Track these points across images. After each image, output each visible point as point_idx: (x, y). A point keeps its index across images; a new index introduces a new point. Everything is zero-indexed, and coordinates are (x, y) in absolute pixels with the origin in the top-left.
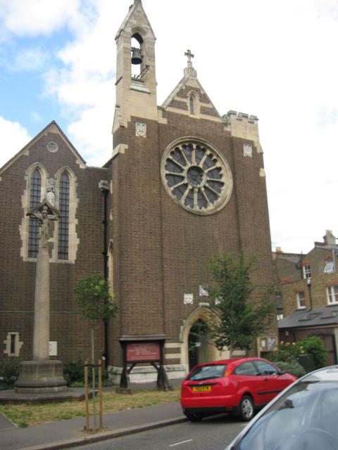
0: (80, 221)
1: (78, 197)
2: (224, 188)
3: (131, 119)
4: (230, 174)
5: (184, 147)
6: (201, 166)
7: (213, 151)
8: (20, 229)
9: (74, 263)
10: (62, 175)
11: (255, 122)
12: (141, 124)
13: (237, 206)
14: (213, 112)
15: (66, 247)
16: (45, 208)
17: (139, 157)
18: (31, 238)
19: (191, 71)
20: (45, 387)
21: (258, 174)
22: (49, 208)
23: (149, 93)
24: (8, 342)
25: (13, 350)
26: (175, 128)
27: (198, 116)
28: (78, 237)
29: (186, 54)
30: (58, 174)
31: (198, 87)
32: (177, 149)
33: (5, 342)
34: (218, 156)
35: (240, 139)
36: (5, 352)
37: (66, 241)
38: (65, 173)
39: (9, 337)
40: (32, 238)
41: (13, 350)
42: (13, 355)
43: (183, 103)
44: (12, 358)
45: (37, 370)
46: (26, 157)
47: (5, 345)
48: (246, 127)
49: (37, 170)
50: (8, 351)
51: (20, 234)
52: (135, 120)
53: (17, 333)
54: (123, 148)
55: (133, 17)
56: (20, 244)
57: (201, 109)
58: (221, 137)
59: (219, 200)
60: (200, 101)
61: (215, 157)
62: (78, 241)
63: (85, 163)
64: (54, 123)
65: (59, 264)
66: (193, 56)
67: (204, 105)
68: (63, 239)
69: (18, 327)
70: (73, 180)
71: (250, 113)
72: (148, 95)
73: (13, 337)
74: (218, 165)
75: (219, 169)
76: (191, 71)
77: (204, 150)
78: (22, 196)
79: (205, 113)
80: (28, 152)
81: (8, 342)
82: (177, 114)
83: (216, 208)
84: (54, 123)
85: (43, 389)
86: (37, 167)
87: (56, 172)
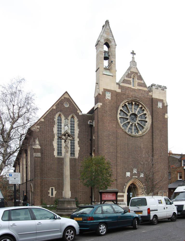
0: (80, 139)
1: (79, 128)
4: (150, 117)
6: (136, 113)
9: (77, 158)
10: (71, 118)
11: (165, 89)
13: (153, 132)
15: (74, 151)
16: (67, 134)
18: (58, 147)
20: (69, 209)
23: (112, 76)
25: (52, 194)
26: (124, 94)
27: (137, 87)
28: (79, 147)
30: (70, 118)
34: (145, 108)
36: (49, 195)
37: (74, 148)
38: (73, 117)
39: (50, 189)
40: (58, 131)
41: (52, 194)
42: (52, 196)
45: (66, 203)
46: (54, 109)
47: (49, 192)
48: (160, 93)
50: (50, 195)
51: (54, 145)
53: (54, 188)
61: (143, 108)
62: (79, 148)
64: (66, 92)
65: (59, 158)
67: (139, 81)
72: (112, 77)
73: (52, 189)
74: (145, 112)
75: (145, 114)
76: (133, 63)
77: (138, 105)
80: (55, 107)
82: (125, 87)
84: (66, 92)
85: (68, 210)
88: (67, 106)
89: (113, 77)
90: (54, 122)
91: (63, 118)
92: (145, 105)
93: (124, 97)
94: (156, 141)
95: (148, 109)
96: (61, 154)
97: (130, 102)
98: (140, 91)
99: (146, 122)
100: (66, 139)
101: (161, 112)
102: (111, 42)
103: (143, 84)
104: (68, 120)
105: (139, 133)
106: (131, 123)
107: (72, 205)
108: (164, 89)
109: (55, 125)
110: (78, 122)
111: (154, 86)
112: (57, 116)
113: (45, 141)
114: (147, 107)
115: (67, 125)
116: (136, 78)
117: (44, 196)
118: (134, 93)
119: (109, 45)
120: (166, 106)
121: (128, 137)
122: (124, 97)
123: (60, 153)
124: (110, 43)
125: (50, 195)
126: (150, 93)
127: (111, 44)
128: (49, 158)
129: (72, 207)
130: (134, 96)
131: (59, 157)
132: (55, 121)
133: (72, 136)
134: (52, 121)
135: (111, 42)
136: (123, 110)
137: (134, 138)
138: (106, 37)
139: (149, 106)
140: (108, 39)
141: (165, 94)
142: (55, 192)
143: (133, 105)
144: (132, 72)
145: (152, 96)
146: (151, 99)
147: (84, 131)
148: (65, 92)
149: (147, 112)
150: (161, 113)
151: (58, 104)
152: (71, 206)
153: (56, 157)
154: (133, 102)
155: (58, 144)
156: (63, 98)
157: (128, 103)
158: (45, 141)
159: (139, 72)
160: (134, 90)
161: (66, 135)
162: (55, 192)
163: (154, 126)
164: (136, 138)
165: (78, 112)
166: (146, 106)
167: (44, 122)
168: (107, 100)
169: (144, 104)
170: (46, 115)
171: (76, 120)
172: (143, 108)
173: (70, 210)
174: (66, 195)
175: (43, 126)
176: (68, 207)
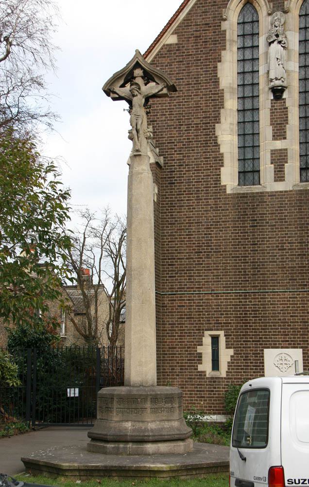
8: (218, 132)
16: (138, 72)
18: (242, 148)
20: (127, 442)
22: (145, 72)
24: (206, 349)
25: (216, 365)
33: (199, 349)
36: (201, 368)
39: (207, 340)
41: (216, 365)
42: (216, 374)
44: (213, 379)
45: (115, 405)
47: (200, 355)
50: (206, 366)
51: (219, 141)
53: (221, 333)
56: (219, 161)
65: (244, 196)
68: (249, 143)
69: (223, 320)
73: (215, 340)
81: (206, 349)
85: (121, 445)
90: (220, 41)
96: (256, 178)
100: (134, 96)
104: (286, 12)
107: (148, 416)
109: (223, 53)
113: (184, 128)
115: (277, 36)
117: (178, 369)
123: (253, 172)
125: (206, 366)
128: (198, 198)
129: (146, 430)
131: (245, 189)
132: (225, 31)
133: (161, 78)
134: (210, 34)
142: (226, 355)
152: (141, 424)
153: (229, 191)
155: (242, 135)
158: (184, 128)
161: (135, 78)
162: (226, 355)
167: (178, 47)
170: (188, 14)
173: (130, 445)
174: (130, 370)
175: (175, 66)
176: (126, 429)
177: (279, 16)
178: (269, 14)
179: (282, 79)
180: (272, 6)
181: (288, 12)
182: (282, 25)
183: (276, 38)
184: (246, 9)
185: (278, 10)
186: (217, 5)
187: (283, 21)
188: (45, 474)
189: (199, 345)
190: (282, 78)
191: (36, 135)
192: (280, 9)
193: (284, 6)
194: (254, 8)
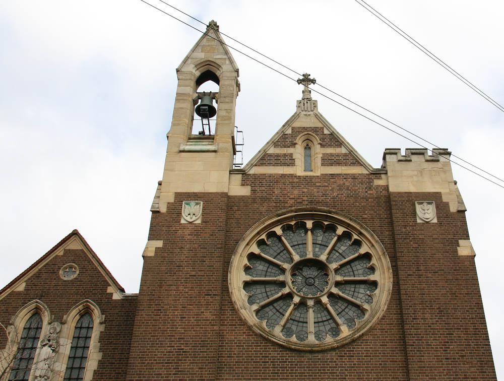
2: (377, 292)
3: (176, 197)
4: (386, 262)
5: (287, 229)
6: (323, 258)
7: (348, 225)
11: (442, 159)
12: (193, 203)
13: (402, 323)
14: (353, 159)
17: (182, 258)
19: (307, 103)
21: (456, 251)
23: (215, 151)
26: (264, 200)
27: (320, 170)
29: (300, 82)
30: (72, 318)
31: (320, 125)
32: (272, 235)
34: (361, 233)
35: (409, 194)
38: (86, 313)
43: (285, 155)
46: (19, 293)
48: (421, 172)
49: (37, 313)
52: (182, 198)
54: (159, 244)
55: (199, 49)
57: (323, 159)
58: (366, 199)
59: (367, 316)
60: (322, 145)
61: (355, 237)
63: (122, 290)
64: (75, 233)
66: (313, 81)
67: (330, 151)
70: (97, 316)
71: (296, 104)
72: (214, 153)
74: (363, 250)
75: (367, 257)
76: (307, 103)
77: (332, 228)
78: (96, 369)
79: (331, 165)
82: (270, 176)
83: (354, 334)
84: (75, 233)
86: (37, 308)
87: (67, 310)
88: (67, 276)
89: (177, 150)
91: (46, 317)
92: (359, 224)
93: (263, 209)
94: (426, 358)
95: (372, 236)
97: (293, 223)
98: (333, 180)
99: (374, 284)
101: (435, 236)
102: (218, 67)
103: (345, 155)
105: (342, 335)
106: (296, 299)
108: (437, 157)
110: (102, 328)
111: (393, 156)
112: (21, 320)
114: (366, 230)
115: (49, 341)
116: (315, 143)
118: (305, 190)
119: (216, 75)
120: (459, 211)
121: (329, 355)
122: (263, 209)
124: (219, 69)
126: (380, 178)
127: (221, 72)
130: (305, 198)
135: (220, 66)
136: (263, 255)
137: (310, 356)
138: (202, 59)
139: (377, 223)
140: (209, 61)
141: (445, 172)
143: (306, 230)
144: (299, 128)
145: (386, 188)
146: (383, 199)
147: (120, 359)
148: (71, 232)
149: (373, 246)
150: (437, 241)
151: (38, 276)
154: (338, 226)
156: (60, 252)
157: (284, 229)
159: (326, 124)
160: (308, 180)
163: (403, 297)
164: (320, 356)
165: (110, 290)
166: (361, 226)
168: (184, 227)
169: (351, 219)
171: (97, 316)
172: (355, 237)
177: (56, 326)
178: (50, 324)
179: (46, 377)
180: (53, 318)
181: (64, 324)
182: (57, 333)
183: (47, 342)
184: (34, 318)
185: (57, 321)
186: (9, 312)
187: (58, 330)
188: (233, 257)
189: (103, 332)
190: (45, 376)
191: (50, 338)
192: (59, 320)
193: (63, 318)
194: (41, 318)
